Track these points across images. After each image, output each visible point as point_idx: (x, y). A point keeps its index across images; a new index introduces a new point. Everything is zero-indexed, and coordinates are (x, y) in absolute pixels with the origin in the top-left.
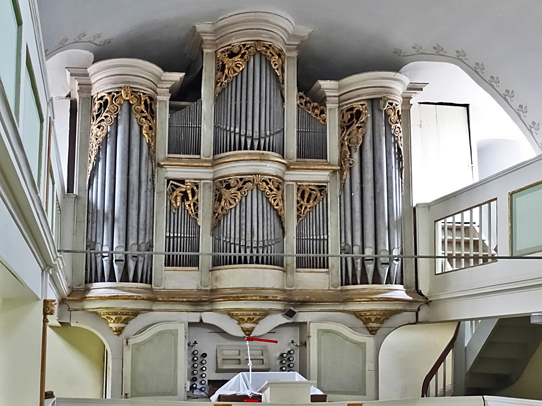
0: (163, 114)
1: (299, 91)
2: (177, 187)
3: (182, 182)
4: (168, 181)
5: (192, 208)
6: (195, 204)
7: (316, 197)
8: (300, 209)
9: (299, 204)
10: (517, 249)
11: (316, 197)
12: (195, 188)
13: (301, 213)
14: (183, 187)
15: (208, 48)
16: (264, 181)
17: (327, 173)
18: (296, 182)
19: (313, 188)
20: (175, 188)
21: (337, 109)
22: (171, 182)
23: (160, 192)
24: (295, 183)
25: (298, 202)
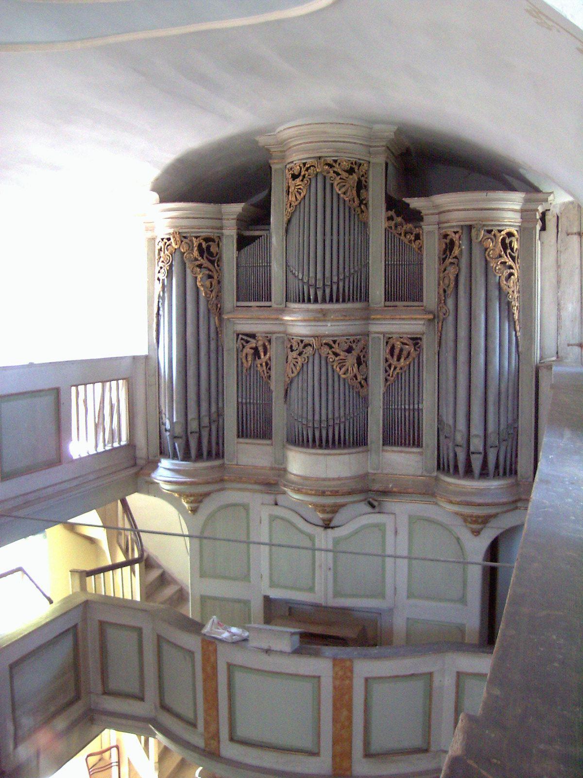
0: (229, 251)
1: (388, 209)
2: (247, 342)
3: (253, 336)
4: (238, 335)
5: (265, 368)
6: (267, 364)
7: (409, 354)
8: (388, 368)
9: (388, 363)
10: (138, 598)
11: (409, 354)
12: (267, 344)
13: (389, 375)
14: (253, 343)
15: (277, 163)
16: (326, 344)
17: (422, 322)
18: (384, 334)
19: (405, 341)
20: (245, 344)
21: (436, 232)
22: (240, 336)
23: (229, 350)
24: (381, 336)
25: (387, 360)
